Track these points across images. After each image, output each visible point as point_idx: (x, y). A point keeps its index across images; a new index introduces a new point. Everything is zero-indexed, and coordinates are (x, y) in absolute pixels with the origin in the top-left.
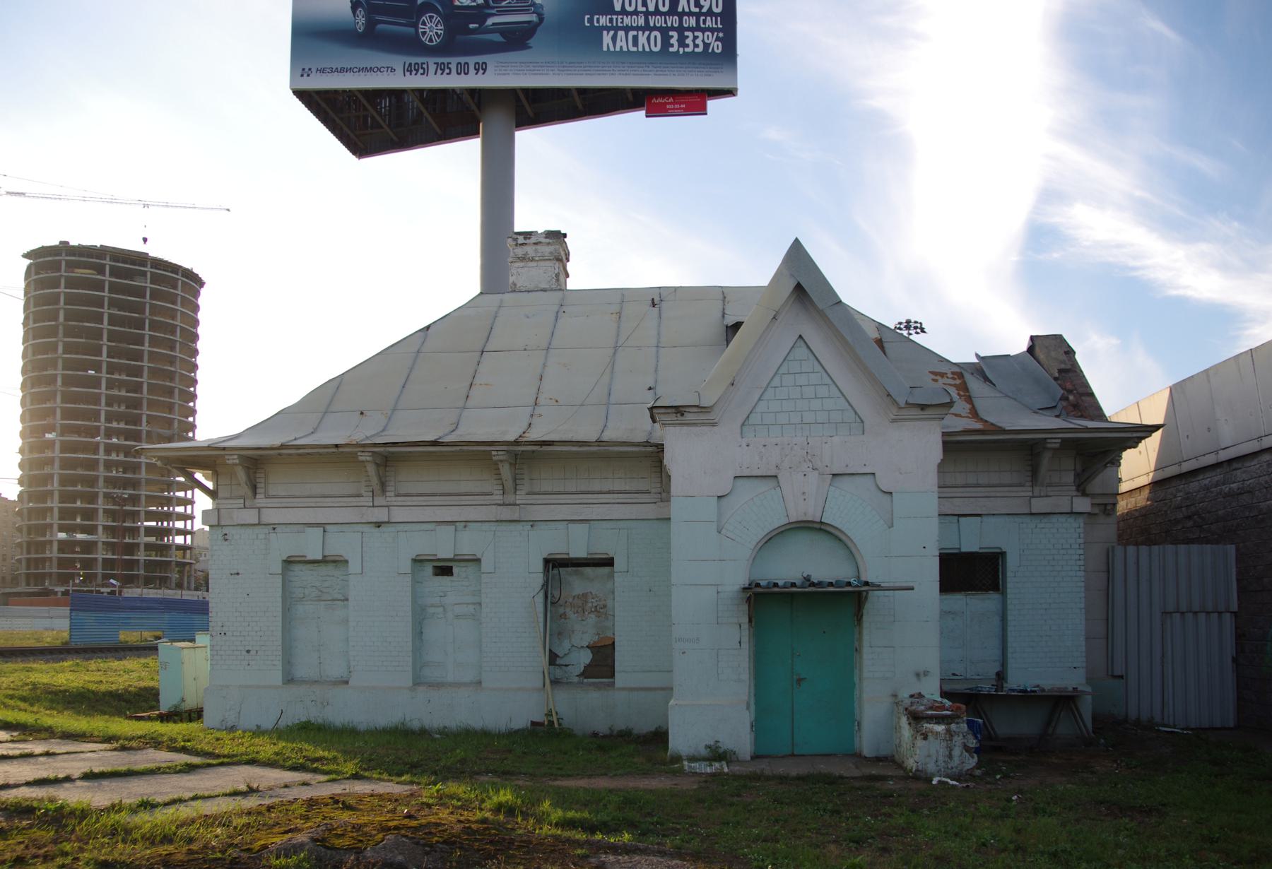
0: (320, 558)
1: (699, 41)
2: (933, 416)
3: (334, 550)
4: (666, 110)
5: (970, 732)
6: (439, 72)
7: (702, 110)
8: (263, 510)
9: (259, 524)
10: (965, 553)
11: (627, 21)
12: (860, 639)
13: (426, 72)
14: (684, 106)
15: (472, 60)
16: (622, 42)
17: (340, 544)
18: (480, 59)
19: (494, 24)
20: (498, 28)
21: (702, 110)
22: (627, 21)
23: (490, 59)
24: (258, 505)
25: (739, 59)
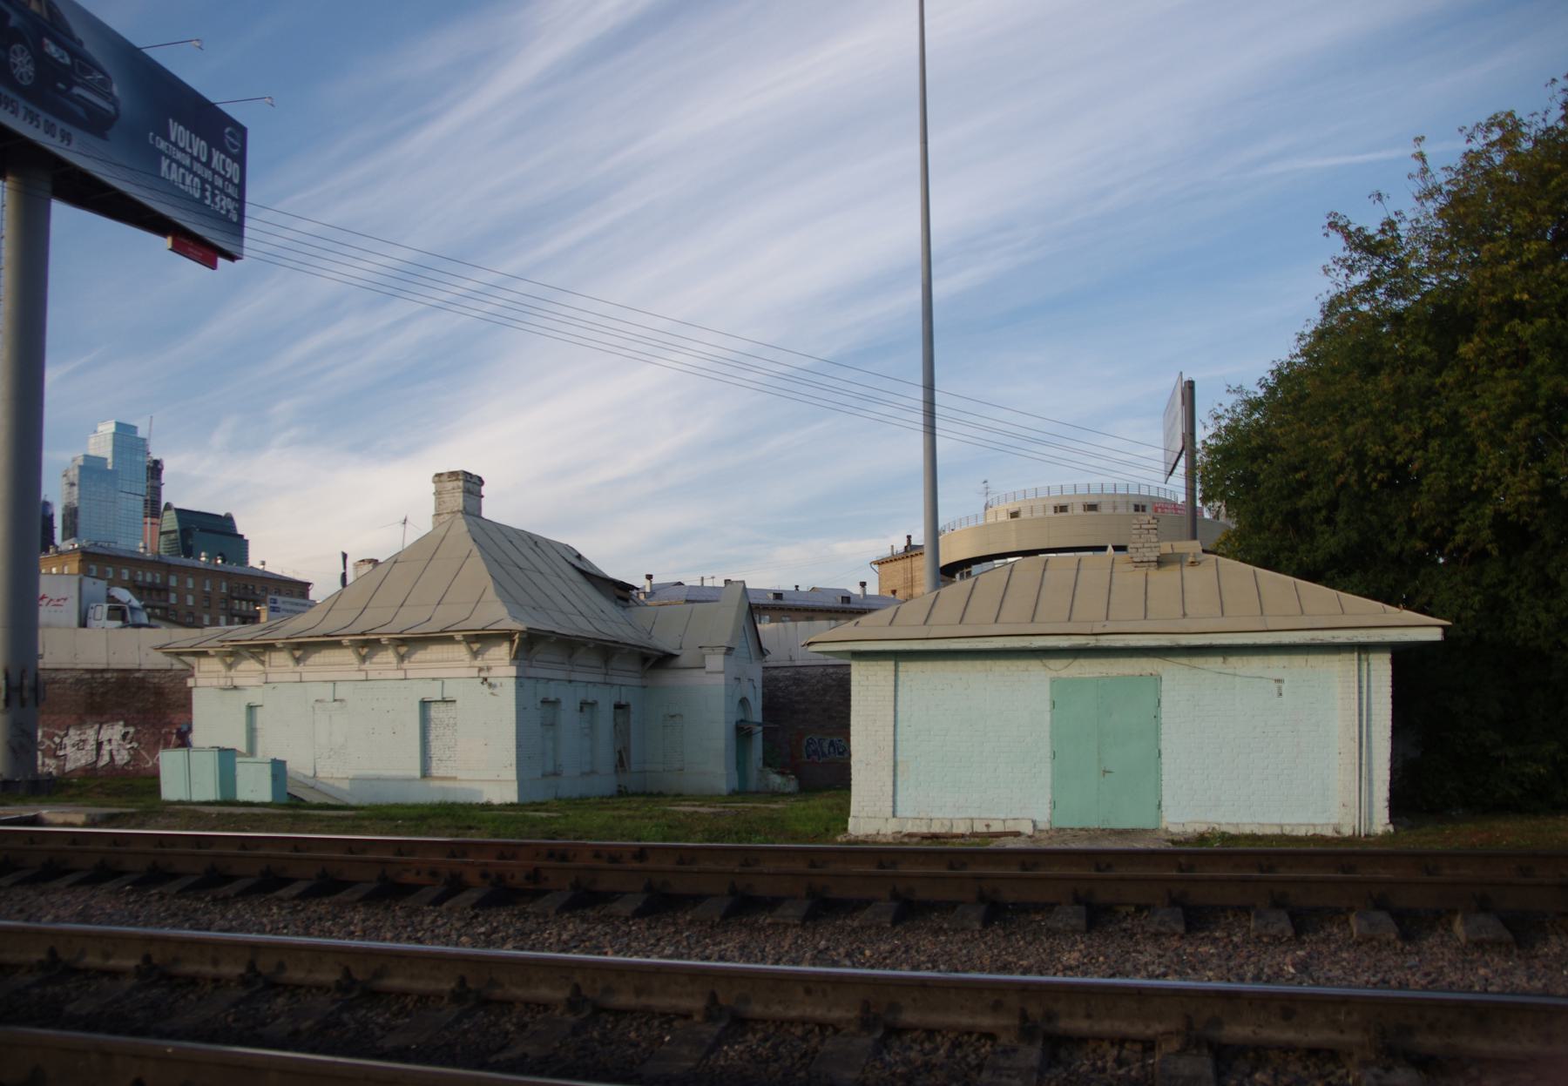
0: (440, 699)
1: (223, 203)
2: (1363, 823)
3: (448, 695)
4: (188, 253)
5: (387, 901)
6: (28, 120)
7: (213, 265)
8: (408, 671)
9: (405, 679)
10: (234, 769)
11: (179, 156)
12: (763, 701)
13: (15, 112)
14: (201, 254)
15: (60, 125)
16: (174, 176)
17: (343, 690)
18: (68, 128)
19: (79, 96)
20: (80, 101)
21: (213, 265)
22: (179, 156)
23: (77, 135)
24: (405, 668)
25: (853, 788)
